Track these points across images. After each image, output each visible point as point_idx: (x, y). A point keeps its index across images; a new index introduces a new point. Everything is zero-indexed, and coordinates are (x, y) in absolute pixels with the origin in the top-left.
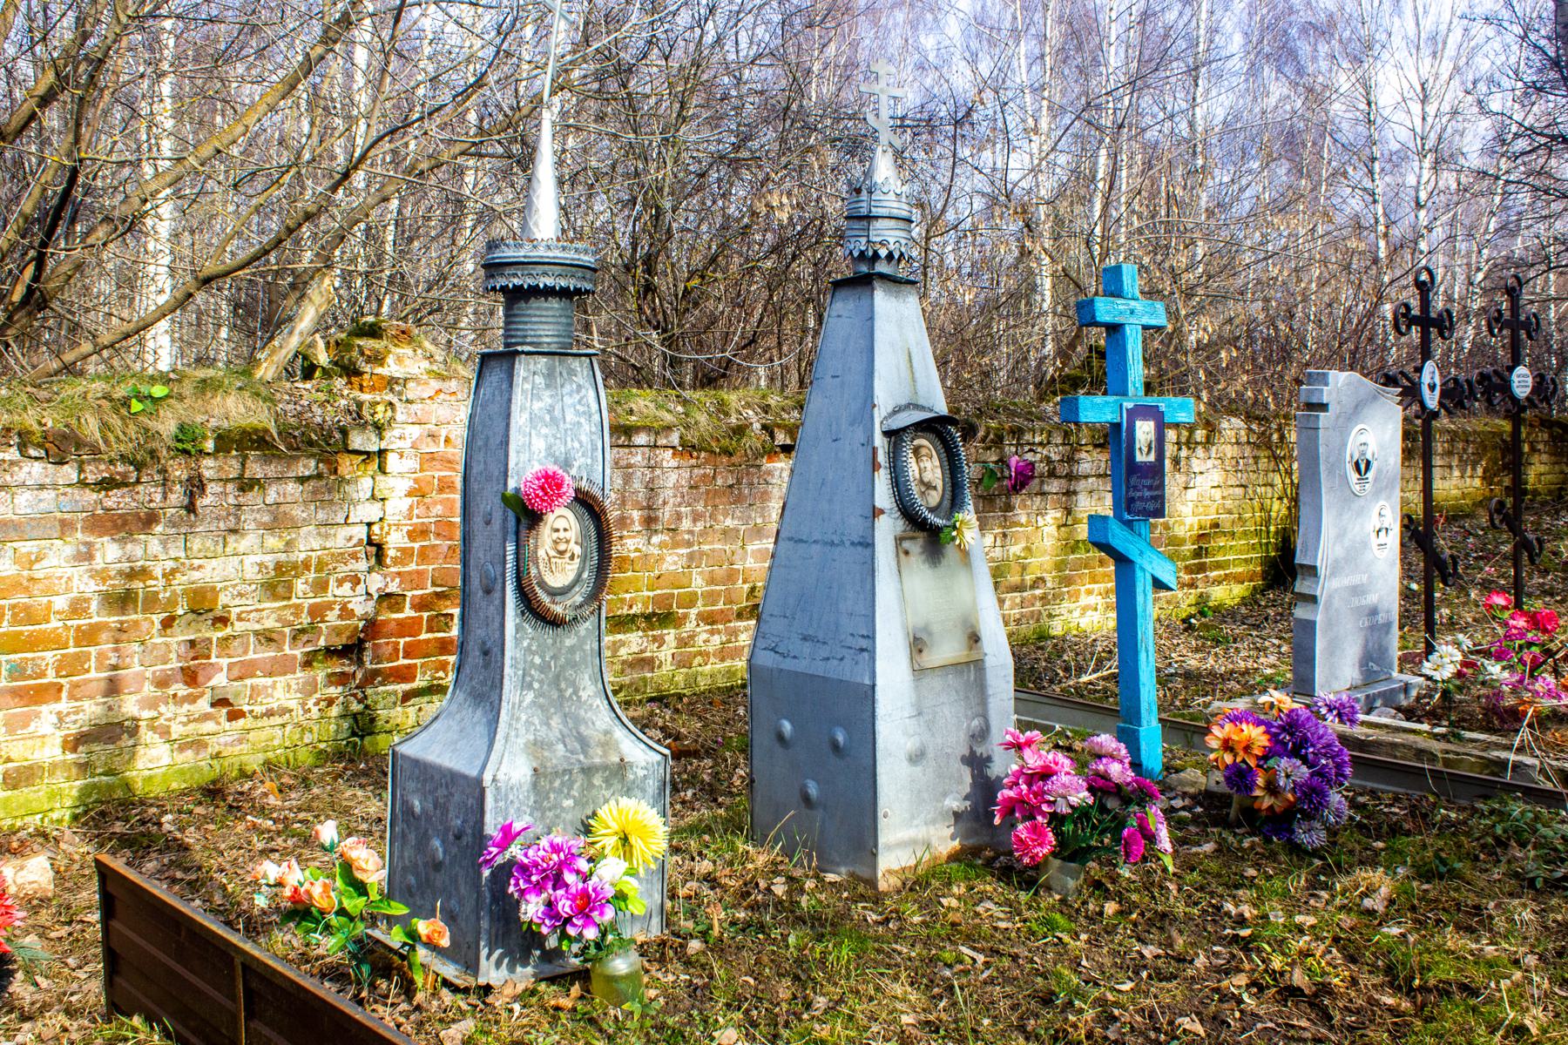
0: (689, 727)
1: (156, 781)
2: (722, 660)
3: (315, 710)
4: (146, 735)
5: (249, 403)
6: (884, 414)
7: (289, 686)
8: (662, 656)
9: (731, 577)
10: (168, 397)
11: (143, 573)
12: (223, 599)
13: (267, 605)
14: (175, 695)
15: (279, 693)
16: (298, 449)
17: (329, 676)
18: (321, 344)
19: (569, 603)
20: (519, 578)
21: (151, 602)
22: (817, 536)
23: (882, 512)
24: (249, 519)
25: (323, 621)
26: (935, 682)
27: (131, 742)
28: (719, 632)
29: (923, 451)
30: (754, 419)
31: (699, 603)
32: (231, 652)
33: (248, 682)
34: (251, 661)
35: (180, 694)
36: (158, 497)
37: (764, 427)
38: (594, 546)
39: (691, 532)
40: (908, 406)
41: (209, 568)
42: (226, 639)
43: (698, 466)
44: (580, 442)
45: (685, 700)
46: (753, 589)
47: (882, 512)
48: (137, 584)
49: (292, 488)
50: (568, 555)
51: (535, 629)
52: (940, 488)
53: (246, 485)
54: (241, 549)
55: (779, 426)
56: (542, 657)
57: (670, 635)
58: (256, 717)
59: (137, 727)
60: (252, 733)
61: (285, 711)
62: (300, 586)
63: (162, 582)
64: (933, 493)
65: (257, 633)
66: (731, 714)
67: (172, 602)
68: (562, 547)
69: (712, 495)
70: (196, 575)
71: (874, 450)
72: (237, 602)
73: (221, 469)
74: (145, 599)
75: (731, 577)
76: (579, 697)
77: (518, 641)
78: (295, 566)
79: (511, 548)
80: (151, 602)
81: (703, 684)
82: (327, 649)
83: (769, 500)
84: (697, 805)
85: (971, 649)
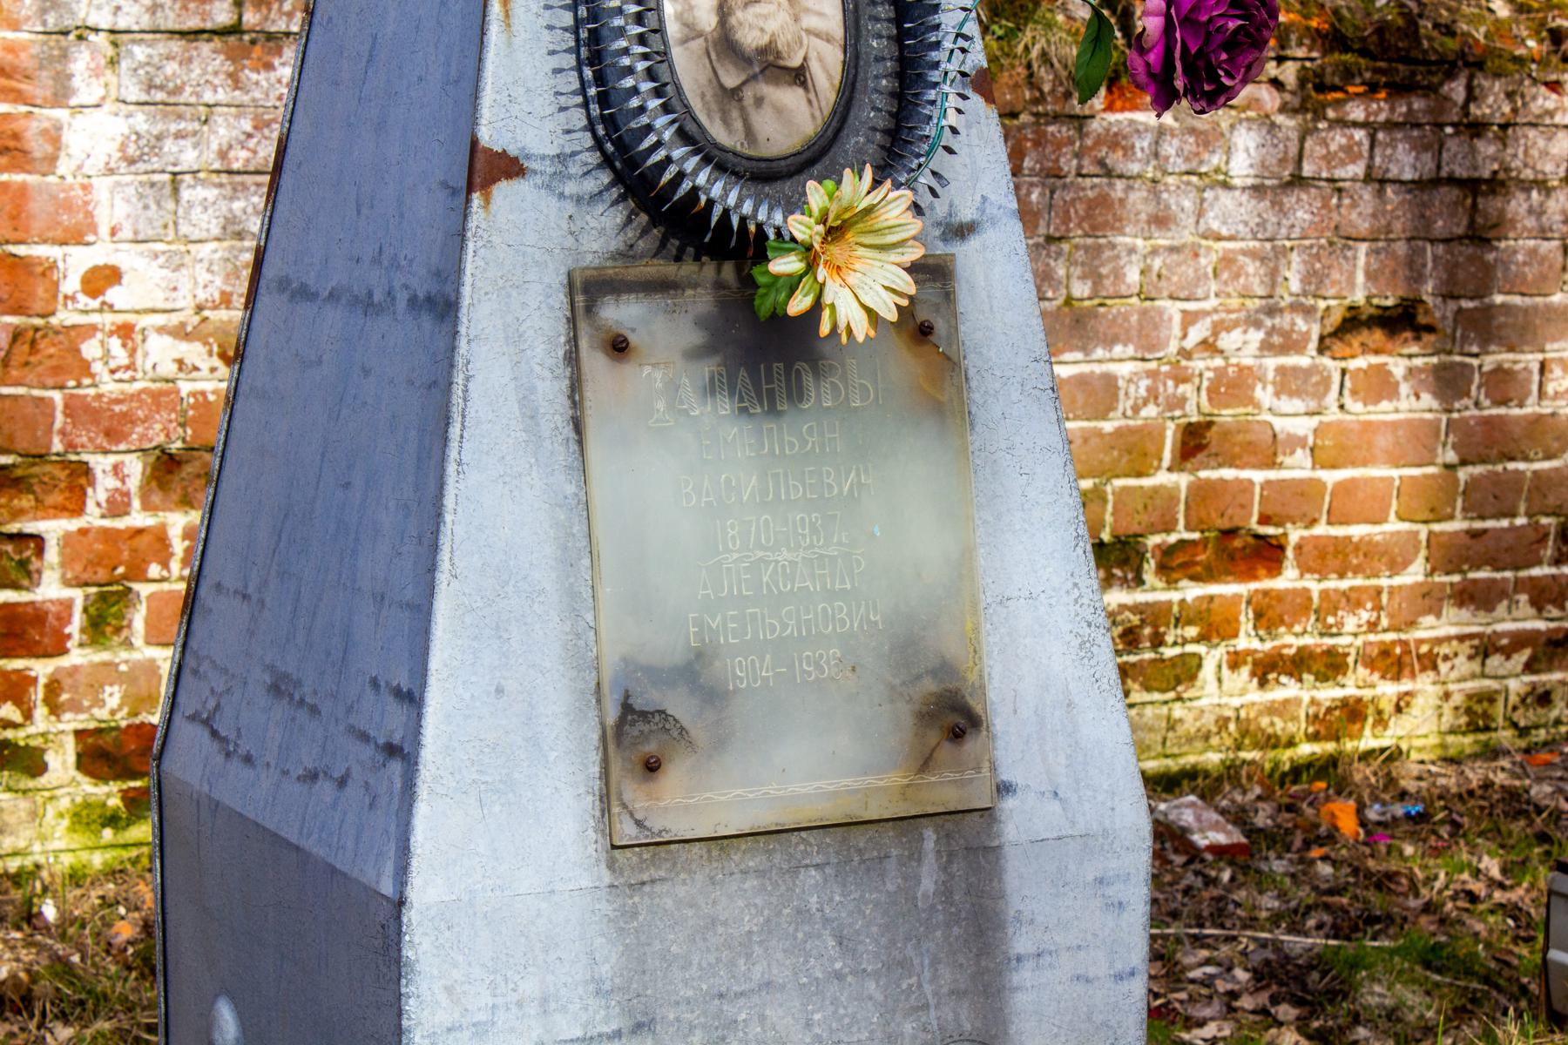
23: (510, 167)
26: (738, 898)
47: (510, 167)
64: (790, 97)
83: (1117, 225)
85: (926, 763)
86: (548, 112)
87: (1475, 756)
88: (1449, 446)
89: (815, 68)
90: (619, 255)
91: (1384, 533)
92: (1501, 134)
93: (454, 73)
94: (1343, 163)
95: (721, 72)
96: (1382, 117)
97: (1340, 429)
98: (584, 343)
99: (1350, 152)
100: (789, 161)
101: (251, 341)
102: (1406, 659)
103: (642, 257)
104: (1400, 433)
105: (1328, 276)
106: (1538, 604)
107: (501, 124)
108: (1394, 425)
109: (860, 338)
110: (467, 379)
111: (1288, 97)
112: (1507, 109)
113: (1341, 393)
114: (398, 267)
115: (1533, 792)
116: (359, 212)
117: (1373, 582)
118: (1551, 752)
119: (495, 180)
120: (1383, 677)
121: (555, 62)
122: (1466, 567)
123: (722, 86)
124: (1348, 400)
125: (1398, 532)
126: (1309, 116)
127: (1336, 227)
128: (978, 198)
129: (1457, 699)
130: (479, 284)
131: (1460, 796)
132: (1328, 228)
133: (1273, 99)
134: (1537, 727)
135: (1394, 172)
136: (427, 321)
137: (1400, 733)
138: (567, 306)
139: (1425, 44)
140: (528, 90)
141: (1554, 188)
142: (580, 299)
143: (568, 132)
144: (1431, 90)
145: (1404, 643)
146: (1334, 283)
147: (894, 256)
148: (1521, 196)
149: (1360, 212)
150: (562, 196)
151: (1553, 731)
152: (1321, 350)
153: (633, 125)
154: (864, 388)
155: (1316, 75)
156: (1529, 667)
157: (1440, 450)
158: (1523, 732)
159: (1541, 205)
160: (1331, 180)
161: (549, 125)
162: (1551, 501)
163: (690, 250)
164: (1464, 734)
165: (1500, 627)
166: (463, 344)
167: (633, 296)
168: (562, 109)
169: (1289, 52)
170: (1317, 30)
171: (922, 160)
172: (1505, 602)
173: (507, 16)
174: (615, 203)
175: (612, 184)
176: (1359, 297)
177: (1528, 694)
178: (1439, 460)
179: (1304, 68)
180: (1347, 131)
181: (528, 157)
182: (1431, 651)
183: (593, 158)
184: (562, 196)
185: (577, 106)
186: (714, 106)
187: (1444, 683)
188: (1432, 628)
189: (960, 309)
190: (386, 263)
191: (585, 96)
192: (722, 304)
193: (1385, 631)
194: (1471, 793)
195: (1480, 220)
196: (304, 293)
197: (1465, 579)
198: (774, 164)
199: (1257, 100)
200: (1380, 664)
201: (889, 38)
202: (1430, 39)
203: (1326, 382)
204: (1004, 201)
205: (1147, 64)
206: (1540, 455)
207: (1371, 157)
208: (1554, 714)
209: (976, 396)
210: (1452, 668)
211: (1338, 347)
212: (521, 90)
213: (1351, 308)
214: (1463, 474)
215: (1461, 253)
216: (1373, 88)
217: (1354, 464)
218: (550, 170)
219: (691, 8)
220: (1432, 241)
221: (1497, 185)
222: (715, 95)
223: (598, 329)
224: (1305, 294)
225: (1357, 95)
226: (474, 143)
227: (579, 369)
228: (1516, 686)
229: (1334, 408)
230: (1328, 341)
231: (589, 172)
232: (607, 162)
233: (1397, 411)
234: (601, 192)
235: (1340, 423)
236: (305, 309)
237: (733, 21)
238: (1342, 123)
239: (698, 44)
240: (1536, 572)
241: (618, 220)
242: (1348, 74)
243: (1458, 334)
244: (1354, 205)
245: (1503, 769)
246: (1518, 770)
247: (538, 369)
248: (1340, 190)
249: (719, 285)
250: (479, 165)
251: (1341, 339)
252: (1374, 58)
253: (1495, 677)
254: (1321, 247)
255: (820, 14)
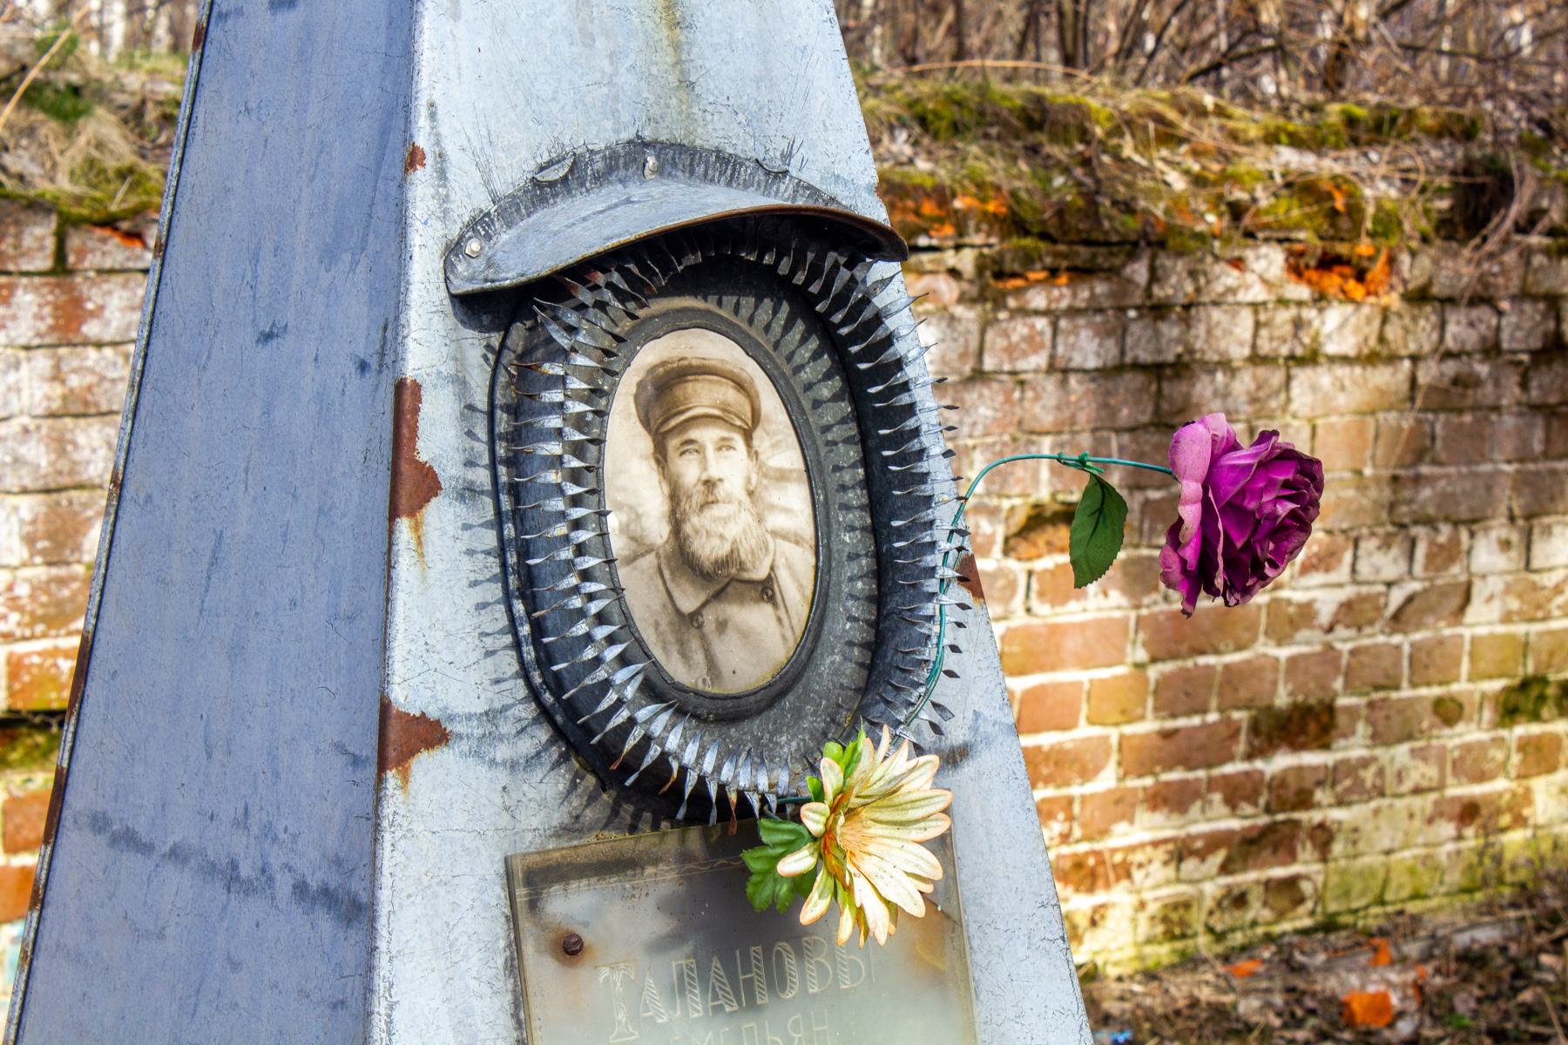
6: (470, 197)
22: (181, 831)
29: (703, 396)
40: (628, 159)
52: (796, 587)
64: (755, 617)
71: (405, 399)
86: (473, 658)
87: (1172, 968)
88: (1139, 644)
89: (784, 579)
90: (566, 831)
91: (1074, 740)
92: (1184, 315)
93: (344, 607)
94: (1025, 354)
95: (676, 594)
96: (1064, 304)
97: (1026, 633)
98: (529, 948)
99: (1032, 342)
100: (759, 696)
101: (54, 884)
102: (1100, 870)
103: (590, 830)
104: (1089, 633)
105: (1012, 474)
106: (1232, 803)
107: (417, 681)
108: (1083, 626)
109: (882, 939)
110: (391, 1007)
111: (965, 286)
112: (1189, 287)
113: (1027, 596)
114: (275, 839)
115: (1242, 1008)
116: (209, 755)
117: (1065, 791)
118: (1251, 958)
119: (413, 753)
120: (1077, 890)
121: (478, 595)
122: (1158, 769)
123: (678, 611)
124: (1035, 603)
125: (1089, 739)
126: (989, 306)
127: (1020, 423)
128: (970, 716)
129: (1153, 908)
130: (399, 885)
131: (1166, 1017)
132: (1011, 423)
133: (951, 290)
134: (1233, 930)
135: (1077, 361)
136: (325, 922)
137: (1096, 947)
138: (505, 902)
139: (1106, 224)
140: (448, 634)
141: (1238, 369)
142: (521, 892)
143: (497, 682)
144: (1112, 272)
145: (1097, 854)
146: (1018, 481)
147: (916, 834)
148: (1205, 378)
149: (1043, 406)
150: (493, 762)
151: (1249, 933)
152: (1007, 551)
153: (588, 681)
154: (854, 963)
155: (994, 261)
156: (1225, 869)
157: (1129, 649)
158: (1219, 937)
159: (1227, 386)
160: (1013, 373)
161: (474, 676)
162: (1243, 694)
163: (647, 815)
164: (1160, 943)
165: (1195, 829)
166: (382, 962)
167: (584, 882)
168: (489, 654)
169: (967, 240)
170: (995, 215)
171: (922, 690)
172: (1198, 804)
173: (420, 543)
174: (556, 765)
175: (551, 742)
176: (1043, 494)
177: (1224, 897)
178: (1129, 659)
179: (981, 255)
180: (1029, 320)
181: (451, 718)
182: (1124, 860)
183: (528, 711)
184: (493, 762)
185: (505, 648)
186: (671, 638)
187: (1139, 892)
188: (1126, 834)
189: (958, 854)
190: (255, 830)
191: (515, 634)
192: (687, 878)
193: (1077, 841)
194: (1178, 1013)
195: (1165, 406)
196: (128, 840)
197: (1157, 782)
198: (742, 701)
199: (935, 292)
200: (1074, 877)
201: (863, 529)
202: (1110, 218)
203: (1012, 585)
204: (999, 716)
205: (1183, 562)
206: (1231, 647)
207: (1054, 346)
208: (1250, 915)
209: (979, 958)
210: (1147, 875)
211: (1023, 547)
212: (440, 635)
213: (1036, 506)
214: (1154, 672)
215: (1147, 442)
216: (1054, 272)
217: (1042, 669)
218: (478, 732)
219: (638, 516)
220: (1118, 431)
221: (1182, 368)
222: (671, 623)
223: (544, 928)
224: (989, 494)
225: (1038, 282)
226: (385, 707)
227: (524, 980)
228: (1212, 889)
229: (1021, 612)
230: (1012, 542)
231: (523, 730)
232: (545, 714)
233: (1085, 610)
234: (538, 754)
235: (1026, 628)
236: (133, 862)
237: (688, 529)
238: (1024, 312)
239: (648, 562)
240: (1229, 769)
241: (561, 787)
242: (1028, 260)
243: (1146, 526)
244: (1037, 398)
245: (1207, 983)
246: (1222, 983)
247: (474, 983)
248: (1022, 383)
249: (685, 857)
250: (394, 734)
251: (1026, 539)
252: (1054, 241)
253: (1191, 882)
254: (1004, 444)
255: (787, 511)
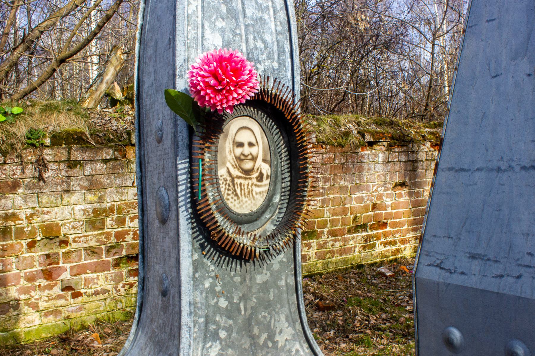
0: (327, 291)
1: (33, 334)
2: (341, 255)
3: (122, 290)
4: (26, 309)
5: (73, 118)
7: (107, 278)
8: (310, 253)
9: (344, 211)
10: (22, 113)
11: (14, 216)
12: (63, 231)
13: (91, 233)
14: (39, 286)
15: (101, 282)
16: (102, 143)
17: (129, 271)
18: (118, 88)
19: (258, 232)
20: (194, 203)
21: (20, 234)
24: (75, 184)
25: (123, 241)
27: (15, 313)
28: (339, 240)
30: (353, 129)
31: (329, 226)
32: (71, 260)
33: (83, 276)
34: (83, 264)
35: (42, 285)
36: (18, 172)
37: (359, 132)
38: (285, 165)
39: (323, 188)
41: (53, 213)
42: (68, 253)
43: (326, 153)
44: (264, 42)
45: (323, 276)
46: (356, 217)
48: (11, 223)
49: (99, 165)
50: (255, 175)
51: (218, 264)
53: (72, 164)
54: (72, 202)
55: (367, 132)
56: (229, 299)
57: (314, 243)
58: (88, 296)
59: (18, 304)
60: (87, 305)
61: (105, 291)
62: (109, 221)
63: (25, 222)
65: (85, 249)
66: (348, 284)
67: (33, 233)
68: (248, 165)
69: (333, 169)
70: (46, 217)
72: (72, 231)
73: (55, 155)
74: (16, 232)
75: (344, 211)
76: (275, 343)
77: (196, 282)
78: (105, 211)
79: (183, 166)
80: (20, 234)
81: (332, 268)
82: (127, 256)
83: (363, 171)
84: (338, 340)
